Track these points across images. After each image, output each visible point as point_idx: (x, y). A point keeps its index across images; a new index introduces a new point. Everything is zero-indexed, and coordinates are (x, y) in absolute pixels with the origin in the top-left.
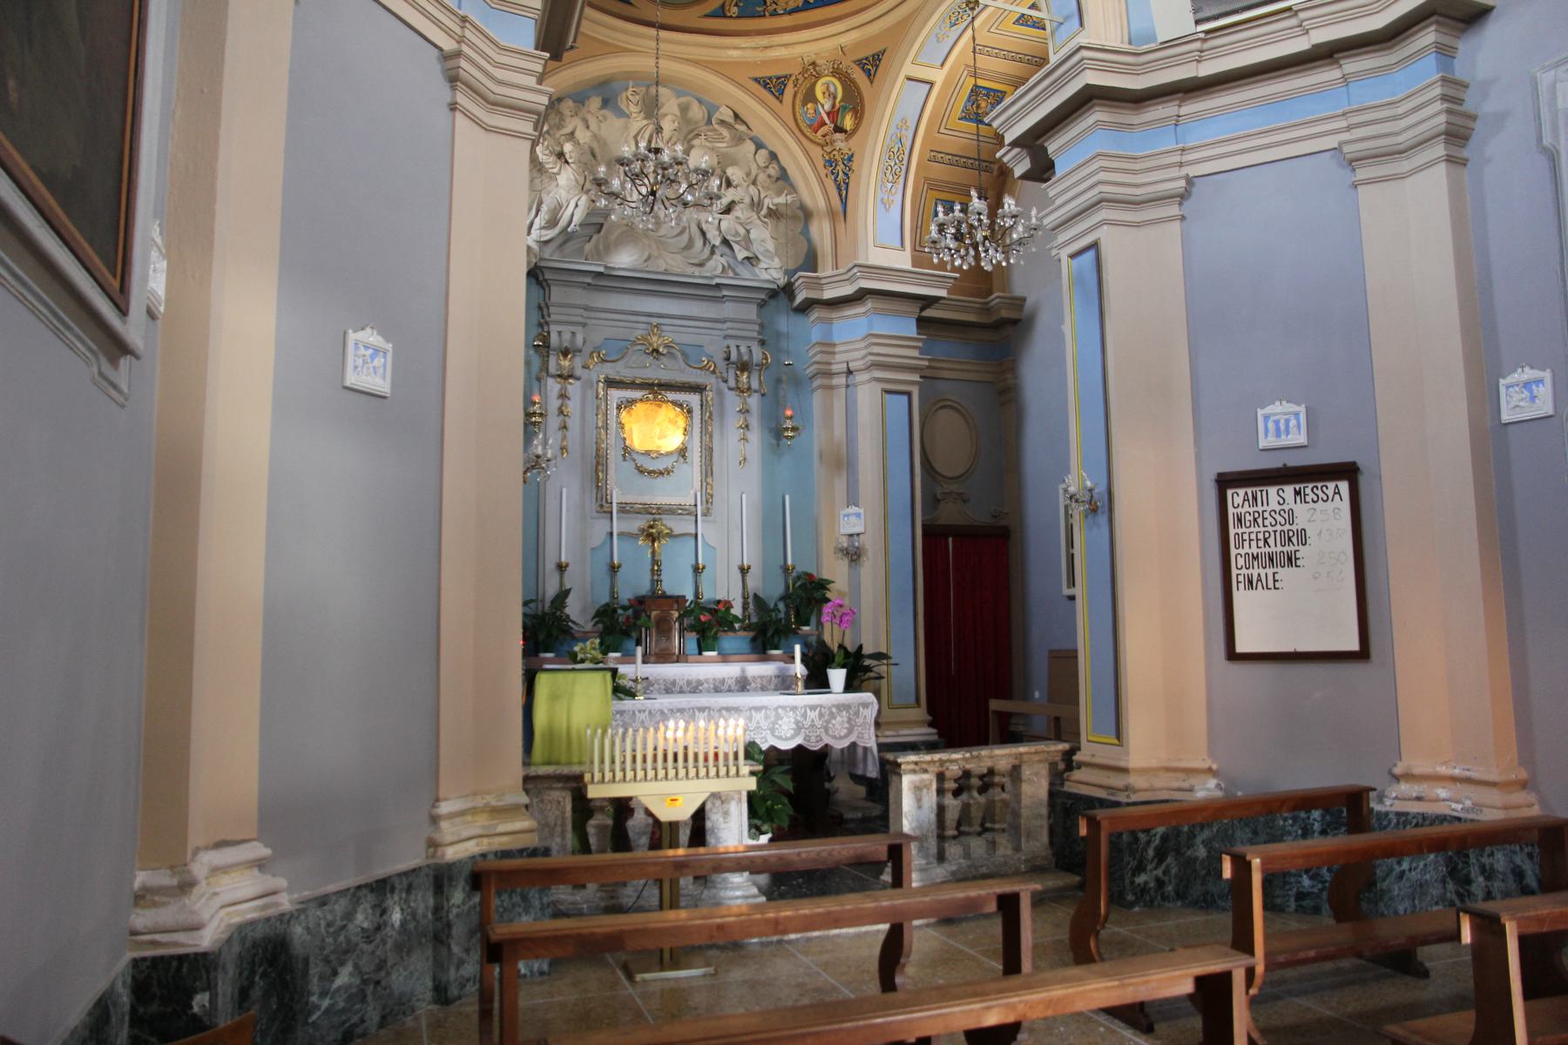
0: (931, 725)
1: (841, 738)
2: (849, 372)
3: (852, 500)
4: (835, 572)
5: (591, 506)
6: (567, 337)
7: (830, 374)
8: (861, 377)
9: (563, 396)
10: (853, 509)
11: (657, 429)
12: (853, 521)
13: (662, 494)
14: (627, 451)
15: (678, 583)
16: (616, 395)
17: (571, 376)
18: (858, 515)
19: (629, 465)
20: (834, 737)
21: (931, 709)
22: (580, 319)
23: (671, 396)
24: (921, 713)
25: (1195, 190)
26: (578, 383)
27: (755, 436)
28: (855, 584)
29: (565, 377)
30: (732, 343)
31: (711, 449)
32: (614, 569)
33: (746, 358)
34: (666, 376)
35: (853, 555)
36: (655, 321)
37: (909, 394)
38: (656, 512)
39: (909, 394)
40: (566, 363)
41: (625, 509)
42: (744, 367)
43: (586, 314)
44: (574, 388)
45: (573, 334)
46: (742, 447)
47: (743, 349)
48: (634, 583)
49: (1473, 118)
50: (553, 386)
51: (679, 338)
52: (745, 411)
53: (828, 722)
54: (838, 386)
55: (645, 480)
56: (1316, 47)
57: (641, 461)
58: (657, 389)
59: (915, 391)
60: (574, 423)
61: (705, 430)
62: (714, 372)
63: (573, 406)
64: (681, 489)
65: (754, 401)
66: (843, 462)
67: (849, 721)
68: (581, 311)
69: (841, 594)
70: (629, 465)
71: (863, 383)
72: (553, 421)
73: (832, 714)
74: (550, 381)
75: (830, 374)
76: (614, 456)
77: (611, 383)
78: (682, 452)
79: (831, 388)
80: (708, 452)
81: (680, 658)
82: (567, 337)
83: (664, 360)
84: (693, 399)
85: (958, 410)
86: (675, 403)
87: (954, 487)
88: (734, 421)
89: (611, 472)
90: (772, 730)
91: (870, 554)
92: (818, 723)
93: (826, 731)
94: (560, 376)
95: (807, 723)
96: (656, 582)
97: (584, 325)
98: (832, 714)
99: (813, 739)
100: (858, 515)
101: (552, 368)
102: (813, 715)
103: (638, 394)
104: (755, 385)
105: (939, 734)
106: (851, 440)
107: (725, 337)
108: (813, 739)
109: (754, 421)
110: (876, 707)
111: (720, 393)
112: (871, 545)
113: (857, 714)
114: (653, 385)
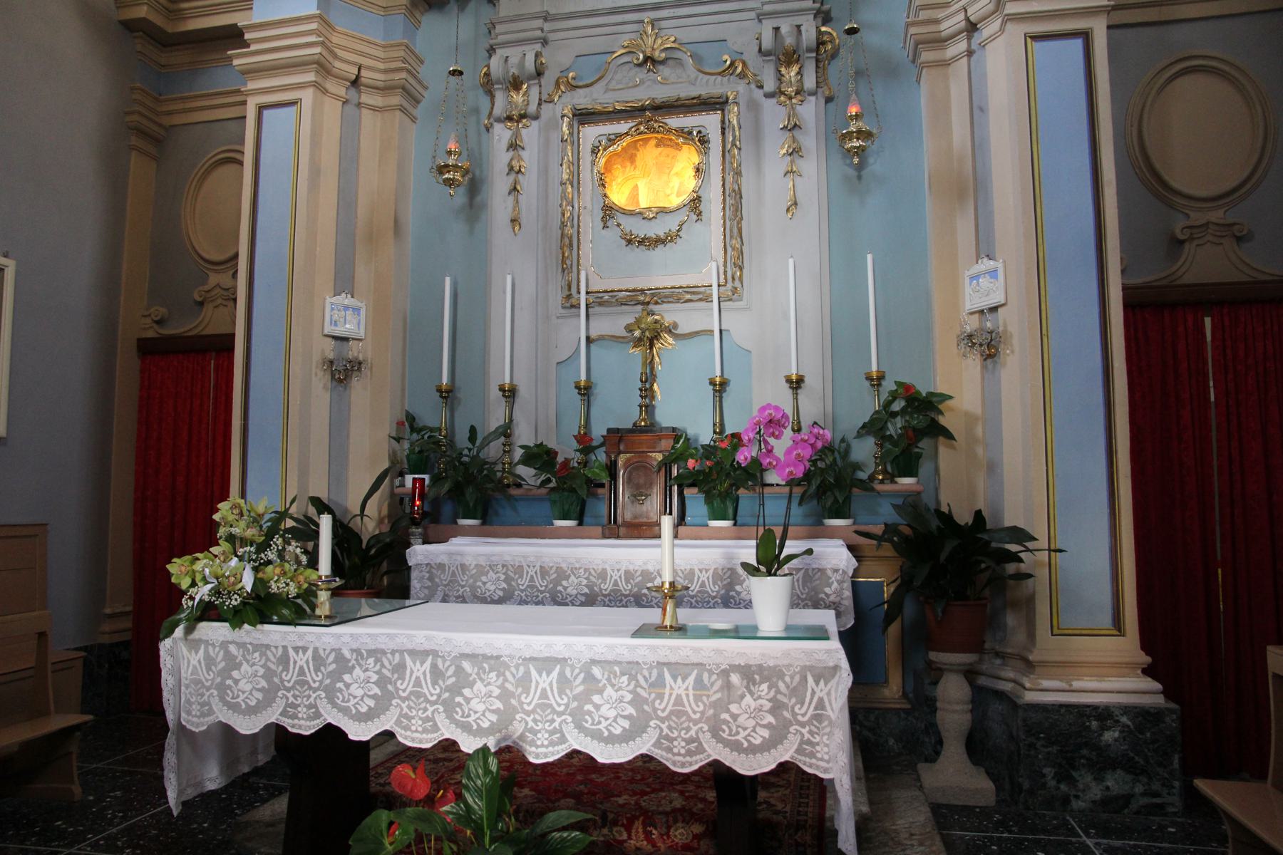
0: (1148, 671)
1: (753, 750)
2: (972, 27)
3: (984, 249)
4: (959, 383)
5: (556, 297)
6: (514, 60)
7: (940, 42)
8: (987, 30)
9: (513, 146)
10: (986, 264)
11: (658, 180)
12: (986, 285)
13: (660, 271)
14: (609, 211)
15: (686, 411)
16: (591, 133)
17: (522, 116)
18: (993, 273)
19: (612, 234)
20: (736, 747)
21: (1147, 644)
22: (538, 33)
23: (675, 122)
24: (1128, 646)
26: (535, 124)
27: (811, 166)
28: (991, 399)
29: (517, 118)
30: (768, 26)
31: (738, 194)
32: (585, 391)
33: (789, 41)
34: (662, 93)
35: (988, 346)
36: (647, 16)
37: (261, 109)
38: (645, 299)
39: (1086, 35)
40: (518, 98)
41: (602, 301)
42: (790, 57)
43: (547, 26)
44: (530, 133)
45: (777, 29)
46: (791, 187)
47: (784, 30)
48: (616, 409)
50: (502, 134)
51: (685, 35)
52: (793, 127)
53: (226, 673)
54: (955, 59)
55: (639, 253)
57: (630, 225)
58: (650, 116)
59: (1099, 28)
60: (529, 183)
61: (732, 171)
62: (742, 76)
63: (529, 158)
64: (697, 261)
65: (809, 110)
66: (969, 187)
67: (777, 707)
68: (539, 23)
69: (971, 419)
70: (612, 234)
71: (993, 38)
72: (499, 184)
73: (229, 657)
74: (498, 128)
75: (940, 42)
76: (590, 223)
77: (584, 117)
78: (695, 204)
79: (945, 64)
80: (734, 200)
81: (644, 530)
82: (514, 60)
83: (665, 71)
84: (709, 122)
85: (1233, 81)
86: (686, 134)
87: (1216, 216)
88: (776, 147)
89: (586, 249)
90: (222, 689)
91: (1015, 342)
92: (694, 709)
93: (715, 733)
94: (509, 118)
95: (665, 706)
96: (648, 409)
97: (545, 42)
98: (229, 657)
99: (679, 746)
100: (993, 273)
101: (498, 111)
102: (680, 688)
103: (623, 127)
104: (810, 82)
105: (1166, 693)
106: (978, 145)
107: (760, 18)
108: (679, 746)
109: (810, 141)
110: (845, 678)
111: (754, 106)
112: (1016, 324)
113: (798, 692)
114: (643, 109)
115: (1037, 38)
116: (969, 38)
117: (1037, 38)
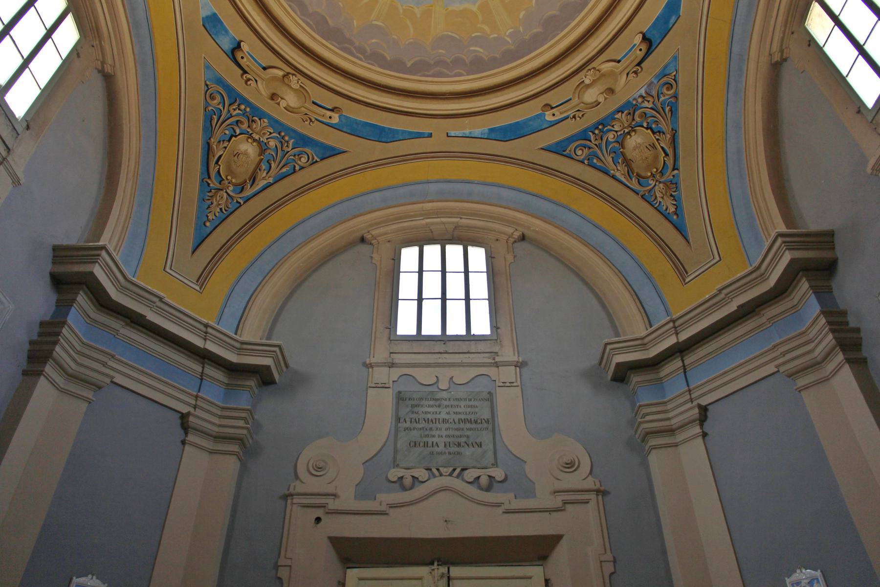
25: (709, 414)
49: (858, 330)
56: (740, 307)
115: (361, 579)
116: (701, 425)
117: (361, 579)
